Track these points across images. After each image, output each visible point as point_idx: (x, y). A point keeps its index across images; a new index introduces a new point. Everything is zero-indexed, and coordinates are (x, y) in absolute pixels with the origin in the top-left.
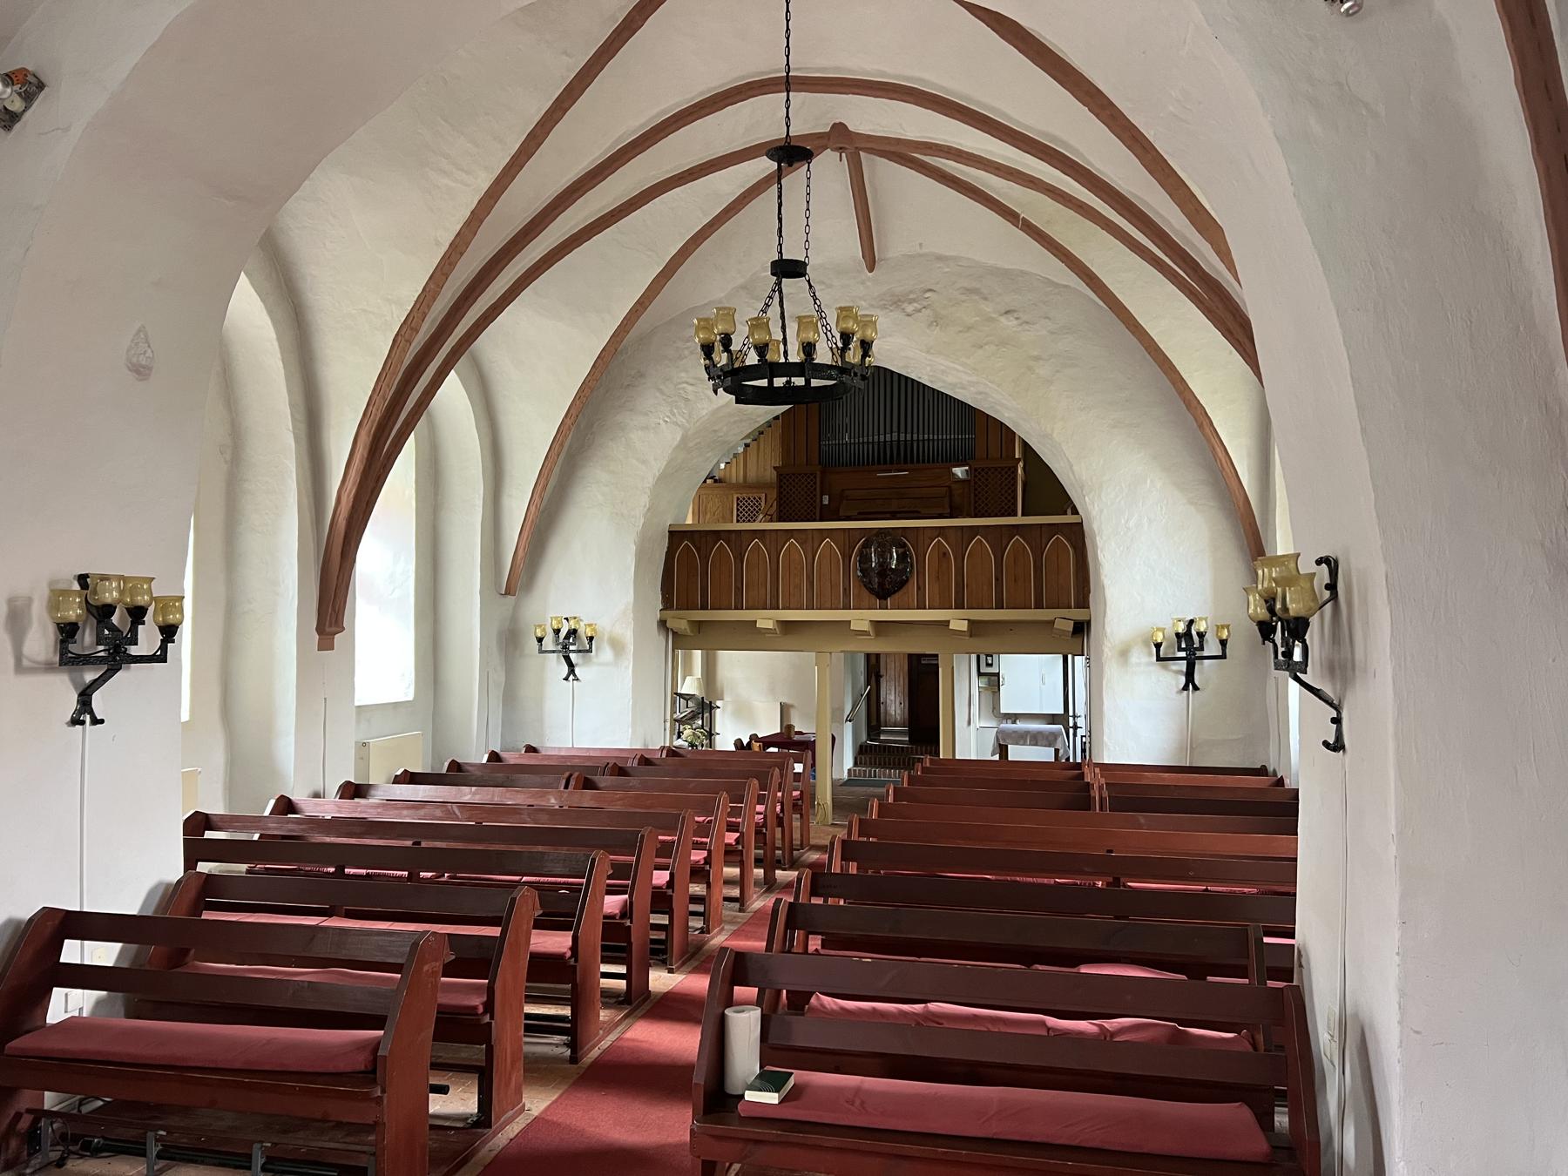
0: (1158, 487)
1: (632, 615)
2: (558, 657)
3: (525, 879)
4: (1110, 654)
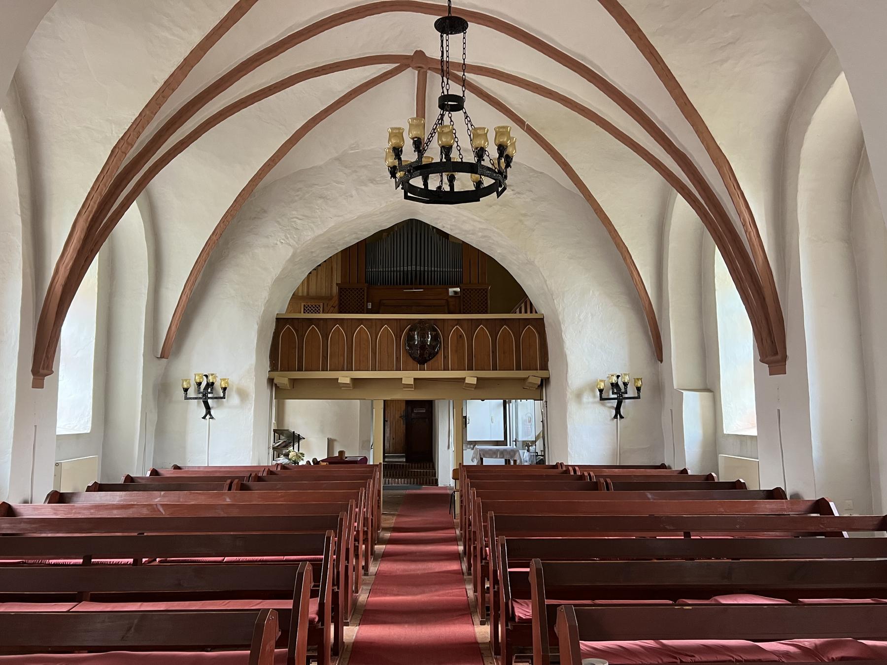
0: (597, 295)
1: (254, 373)
2: (198, 403)
3: (226, 559)
4: (571, 397)
